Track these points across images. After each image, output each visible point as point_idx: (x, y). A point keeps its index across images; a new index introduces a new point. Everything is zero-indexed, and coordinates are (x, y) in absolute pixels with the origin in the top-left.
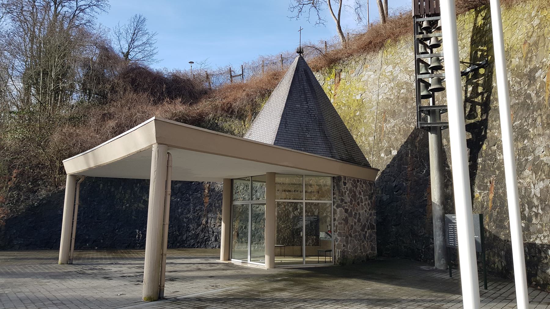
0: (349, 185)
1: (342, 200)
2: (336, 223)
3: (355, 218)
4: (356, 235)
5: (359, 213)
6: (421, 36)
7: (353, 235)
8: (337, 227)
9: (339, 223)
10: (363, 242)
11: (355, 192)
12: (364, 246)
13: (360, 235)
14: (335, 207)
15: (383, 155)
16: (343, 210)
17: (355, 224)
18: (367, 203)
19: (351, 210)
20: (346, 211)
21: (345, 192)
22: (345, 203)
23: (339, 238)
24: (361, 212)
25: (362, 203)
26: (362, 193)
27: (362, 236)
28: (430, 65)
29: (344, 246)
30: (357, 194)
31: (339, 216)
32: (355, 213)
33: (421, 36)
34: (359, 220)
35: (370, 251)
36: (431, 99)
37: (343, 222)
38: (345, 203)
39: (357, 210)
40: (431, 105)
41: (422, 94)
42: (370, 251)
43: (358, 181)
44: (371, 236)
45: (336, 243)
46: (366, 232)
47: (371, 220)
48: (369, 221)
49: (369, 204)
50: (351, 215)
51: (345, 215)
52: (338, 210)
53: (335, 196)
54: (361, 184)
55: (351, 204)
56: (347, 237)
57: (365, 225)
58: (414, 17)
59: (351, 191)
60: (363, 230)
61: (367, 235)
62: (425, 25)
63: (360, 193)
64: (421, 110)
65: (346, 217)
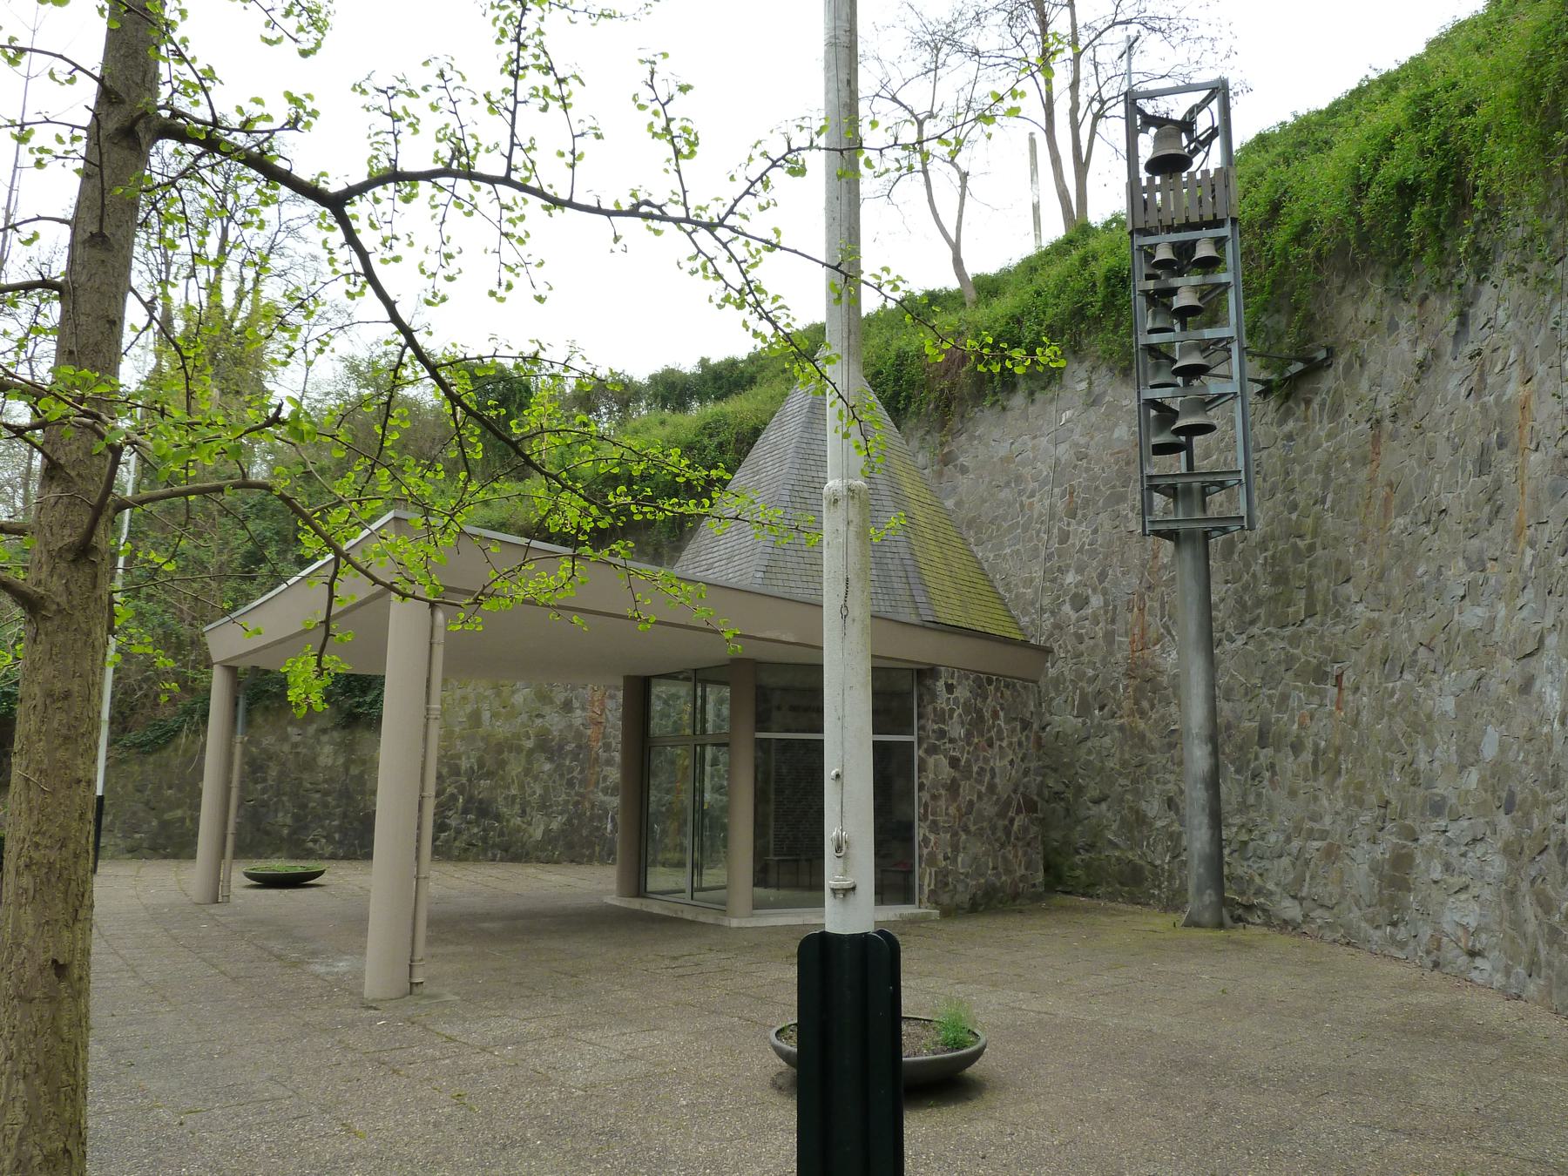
0: (962, 693)
1: (942, 734)
2: (926, 796)
3: (980, 782)
4: (982, 829)
5: (992, 769)
6: (1151, 285)
7: (973, 828)
8: (926, 805)
9: (934, 797)
10: (1002, 846)
11: (979, 712)
12: (1005, 858)
13: (994, 829)
14: (921, 753)
15: (1067, 608)
16: (945, 762)
17: (980, 797)
18: (1015, 740)
19: (968, 760)
20: (954, 763)
21: (952, 711)
22: (951, 741)
23: (932, 837)
24: (998, 764)
25: (1002, 740)
26: (1002, 714)
27: (1000, 834)
28: (1175, 361)
29: (946, 858)
30: (987, 715)
31: (931, 776)
32: (982, 769)
33: (1151, 285)
34: (992, 788)
35: (1023, 871)
36: (1183, 454)
37: (943, 792)
38: (951, 741)
39: (986, 760)
40: (1184, 470)
41: (1155, 440)
42: (1023, 871)
43: (990, 682)
44: (1025, 829)
45: (925, 851)
46: (1012, 821)
47: (1026, 787)
48: (1021, 789)
49: (1020, 744)
50: (967, 773)
51: (946, 772)
52: (931, 761)
53: (923, 722)
54: (997, 689)
55: (969, 744)
56: (955, 834)
57: (1008, 804)
58: (1131, 233)
59: (967, 707)
60: (1002, 814)
61: (1015, 827)
62: (1163, 253)
63: (995, 715)
64: (1152, 485)
65: (954, 780)
